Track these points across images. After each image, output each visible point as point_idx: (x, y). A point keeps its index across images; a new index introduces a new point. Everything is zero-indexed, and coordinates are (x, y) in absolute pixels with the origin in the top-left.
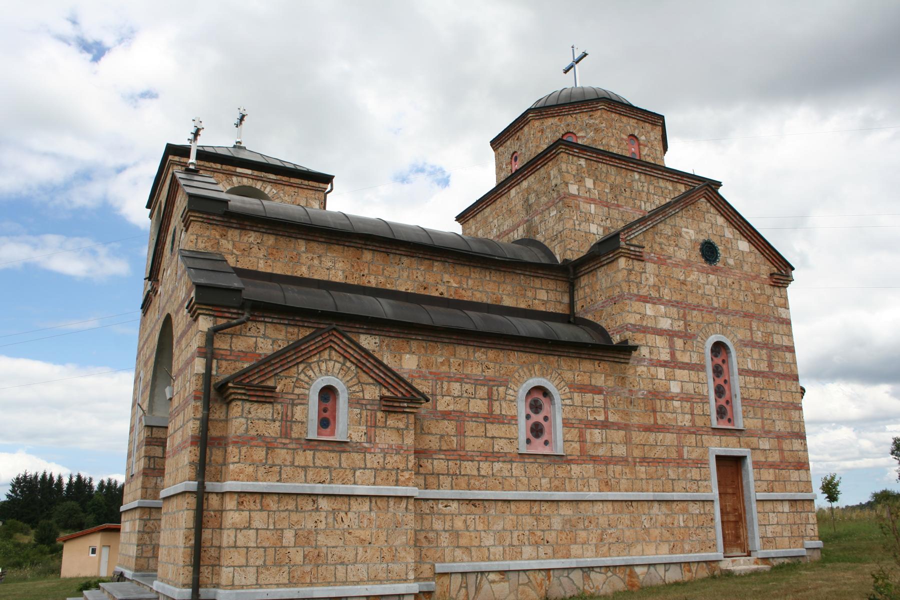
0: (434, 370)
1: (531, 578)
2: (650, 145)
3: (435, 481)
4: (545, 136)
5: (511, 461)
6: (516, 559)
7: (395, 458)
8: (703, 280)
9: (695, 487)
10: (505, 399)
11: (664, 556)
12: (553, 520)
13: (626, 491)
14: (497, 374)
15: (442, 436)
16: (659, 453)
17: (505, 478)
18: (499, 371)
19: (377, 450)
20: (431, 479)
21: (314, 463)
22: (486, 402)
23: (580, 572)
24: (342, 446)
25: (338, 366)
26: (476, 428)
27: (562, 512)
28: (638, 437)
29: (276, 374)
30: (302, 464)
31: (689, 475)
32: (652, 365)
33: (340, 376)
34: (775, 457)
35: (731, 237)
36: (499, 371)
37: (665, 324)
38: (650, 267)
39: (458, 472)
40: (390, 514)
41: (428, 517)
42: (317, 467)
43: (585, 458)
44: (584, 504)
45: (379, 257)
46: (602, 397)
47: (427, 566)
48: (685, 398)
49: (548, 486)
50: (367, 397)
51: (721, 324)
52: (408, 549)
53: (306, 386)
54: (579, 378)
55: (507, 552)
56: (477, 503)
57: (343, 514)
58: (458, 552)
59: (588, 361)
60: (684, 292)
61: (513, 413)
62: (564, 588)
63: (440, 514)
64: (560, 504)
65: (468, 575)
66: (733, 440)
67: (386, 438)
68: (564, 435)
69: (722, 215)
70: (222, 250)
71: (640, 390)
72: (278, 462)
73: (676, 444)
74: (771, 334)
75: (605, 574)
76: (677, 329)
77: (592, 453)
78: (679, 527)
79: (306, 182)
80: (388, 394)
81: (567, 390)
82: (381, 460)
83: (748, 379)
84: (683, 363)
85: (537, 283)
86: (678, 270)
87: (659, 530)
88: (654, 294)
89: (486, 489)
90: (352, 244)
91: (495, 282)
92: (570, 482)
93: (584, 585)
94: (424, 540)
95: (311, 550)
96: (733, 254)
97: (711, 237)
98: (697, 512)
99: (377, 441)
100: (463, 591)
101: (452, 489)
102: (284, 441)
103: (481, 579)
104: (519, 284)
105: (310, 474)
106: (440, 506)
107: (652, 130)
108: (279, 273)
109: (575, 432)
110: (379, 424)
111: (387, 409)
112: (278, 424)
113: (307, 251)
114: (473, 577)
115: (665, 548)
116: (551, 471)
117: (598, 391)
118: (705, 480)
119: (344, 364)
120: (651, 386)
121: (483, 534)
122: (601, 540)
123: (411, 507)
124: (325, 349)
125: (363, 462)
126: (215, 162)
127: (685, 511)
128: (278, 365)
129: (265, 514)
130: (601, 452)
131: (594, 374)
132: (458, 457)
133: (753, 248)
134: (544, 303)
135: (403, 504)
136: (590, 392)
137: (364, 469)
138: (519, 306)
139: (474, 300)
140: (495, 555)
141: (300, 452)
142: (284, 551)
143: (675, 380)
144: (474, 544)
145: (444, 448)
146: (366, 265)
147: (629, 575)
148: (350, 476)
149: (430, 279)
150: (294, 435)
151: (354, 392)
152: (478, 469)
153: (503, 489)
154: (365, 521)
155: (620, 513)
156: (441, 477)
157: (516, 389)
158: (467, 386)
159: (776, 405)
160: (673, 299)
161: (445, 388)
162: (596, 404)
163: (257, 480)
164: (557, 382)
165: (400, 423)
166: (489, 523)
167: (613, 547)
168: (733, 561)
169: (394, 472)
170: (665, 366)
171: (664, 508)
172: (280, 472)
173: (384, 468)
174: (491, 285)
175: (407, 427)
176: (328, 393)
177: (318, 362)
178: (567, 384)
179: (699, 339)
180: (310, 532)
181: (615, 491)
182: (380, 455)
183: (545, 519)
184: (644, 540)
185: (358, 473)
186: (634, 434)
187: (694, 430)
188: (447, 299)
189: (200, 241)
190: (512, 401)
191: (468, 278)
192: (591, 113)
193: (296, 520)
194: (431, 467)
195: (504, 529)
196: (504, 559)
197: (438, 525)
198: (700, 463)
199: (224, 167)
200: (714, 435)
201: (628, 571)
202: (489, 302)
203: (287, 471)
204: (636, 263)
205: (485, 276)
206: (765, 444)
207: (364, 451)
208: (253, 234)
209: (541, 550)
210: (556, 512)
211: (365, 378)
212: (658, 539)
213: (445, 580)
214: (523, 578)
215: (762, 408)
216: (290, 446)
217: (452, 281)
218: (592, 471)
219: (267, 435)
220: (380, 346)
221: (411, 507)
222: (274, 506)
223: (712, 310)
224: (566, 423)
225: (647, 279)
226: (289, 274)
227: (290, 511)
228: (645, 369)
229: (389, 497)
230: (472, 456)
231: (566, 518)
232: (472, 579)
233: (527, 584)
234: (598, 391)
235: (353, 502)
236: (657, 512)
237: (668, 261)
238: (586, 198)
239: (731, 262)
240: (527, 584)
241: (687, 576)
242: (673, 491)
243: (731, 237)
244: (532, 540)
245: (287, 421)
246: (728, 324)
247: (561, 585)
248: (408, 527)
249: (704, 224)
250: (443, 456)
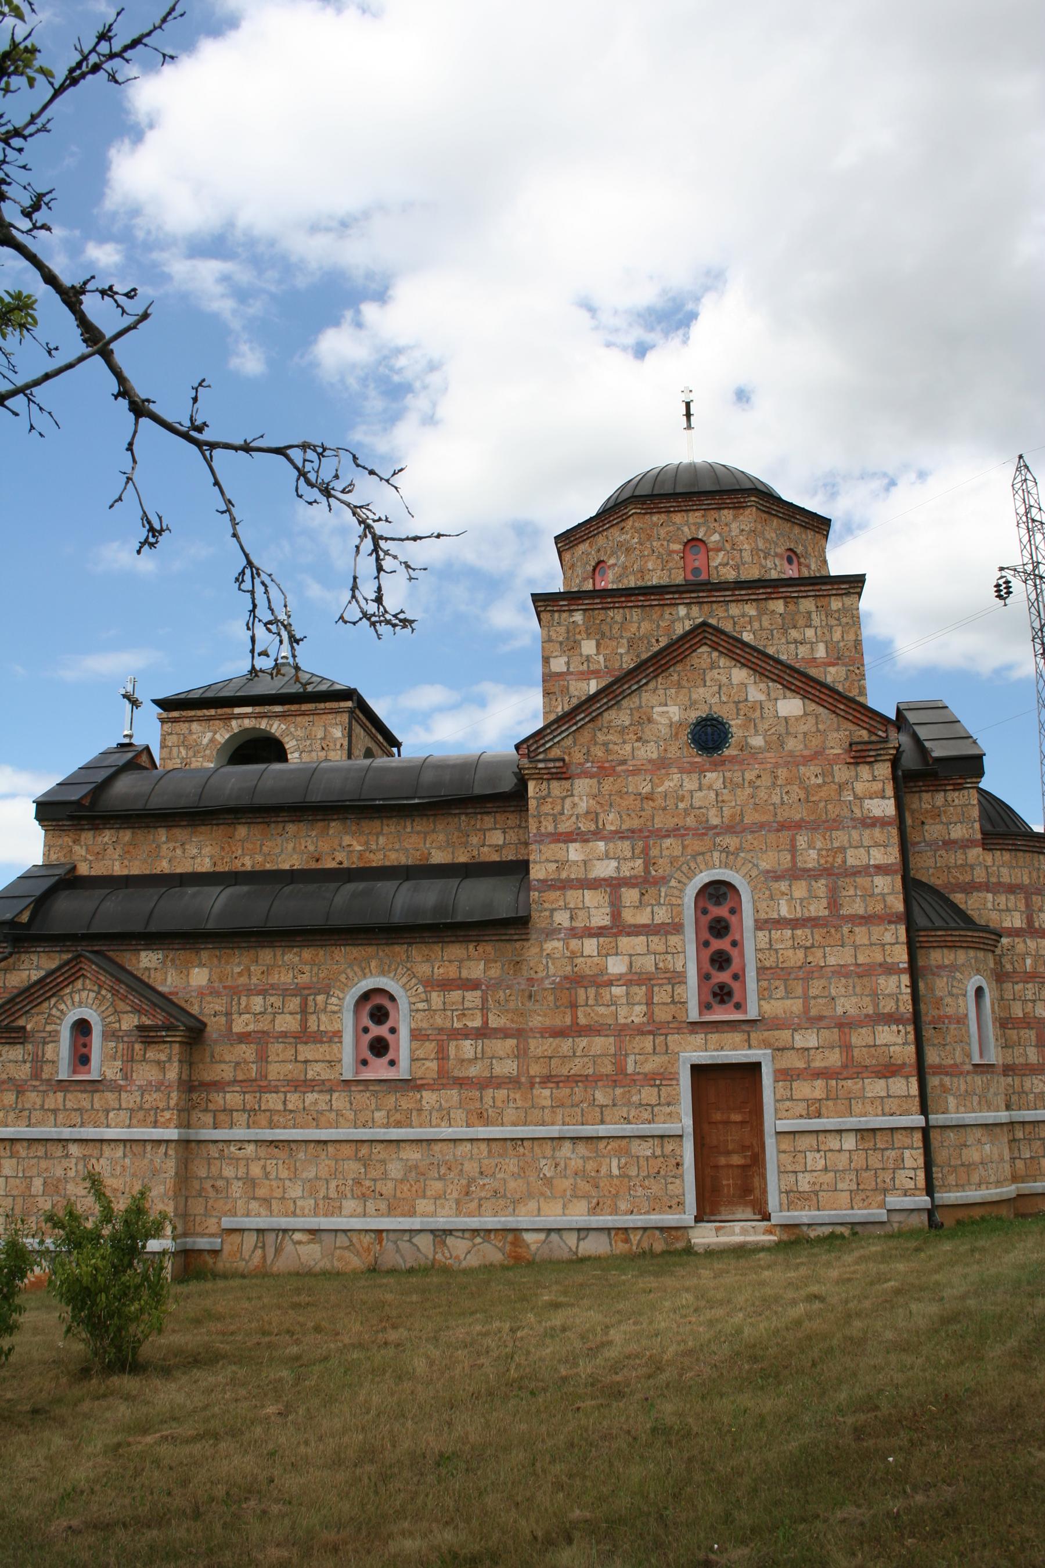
0: (229, 984)
1: (355, 1240)
2: (728, 546)
3: (227, 1119)
4: (575, 573)
5: (331, 1091)
6: (332, 1215)
7: (155, 1096)
8: (690, 783)
9: (646, 1115)
10: (325, 1010)
11: (578, 1216)
12: (390, 1166)
13: (514, 1124)
14: (315, 979)
15: (238, 1064)
16: (576, 1067)
17: (321, 1112)
18: (317, 974)
19: (134, 1088)
20: (222, 1117)
21: (64, 1106)
22: (299, 1017)
23: (431, 1237)
24: (94, 1086)
25: (92, 995)
26: (284, 1051)
27: (403, 1155)
28: (538, 1046)
29: (27, 1012)
30: (52, 1107)
31: (635, 1099)
32: (574, 936)
33: (94, 1007)
34: (834, 1059)
35: (762, 697)
36: (317, 974)
37: (605, 869)
38: (582, 786)
39: (257, 1107)
40: (146, 1161)
41: (216, 1161)
42: (67, 1110)
43: (444, 1081)
44: (440, 1145)
45: (256, 830)
46: (479, 993)
47: (214, 1220)
48: (634, 979)
49: (385, 1121)
50: (124, 1028)
51: (726, 850)
52: (166, 1201)
53: (58, 1021)
54: (441, 970)
55: (321, 1206)
56: (281, 1145)
57: (94, 1161)
58: (254, 1205)
59: (457, 946)
60: (648, 812)
61: (337, 1027)
62: (402, 1256)
63: (232, 1159)
64: (402, 1145)
65: (266, 1233)
66: (738, 1037)
67: (146, 1074)
68: (412, 1051)
69: (744, 665)
70: (76, 858)
71: (548, 976)
72: (27, 1106)
73: (612, 1051)
74: (842, 849)
75: (472, 1240)
76: (628, 874)
77: (457, 1073)
78: (611, 1176)
79: (322, 705)
80: (148, 1022)
81: (421, 989)
82: (138, 1099)
83: (776, 934)
84: (635, 926)
85: (488, 821)
86: (638, 778)
87: (572, 1181)
88: (585, 826)
89: (294, 1127)
90: (221, 821)
91: (418, 833)
92: (419, 1115)
93: (435, 1253)
94: (210, 1190)
95: (60, 1199)
96: (762, 726)
97: (715, 709)
98: (649, 1153)
99: (134, 1077)
100: (259, 1252)
101: (249, 1127)
102: (34, 1083)
103: (283, 1239)
104: (459, 829)
105: (61, 1116)
106: (232, 1149)
107: (735, 517)
108: (136, 873)
109: (430, 1047)
110: (137, 1058)
111: (144, 1039)
112: (28, 1065)
113: (168, 840)
114: (273, 1235)
115: (582, 1206)
116: (391, 1100)
117: (473, 985)
118: (669, 1104)
119: (98, 993)
120: (569, 968)
121: (287, 1182)
122: (467, 1194)
123: (171, 1152)
124: (78, 978)
125: (117, 1102)
126: (208, 708)
127: (619, 1153)
128: (25, 1003)
129: (14, 1161)
130: (473, 1071)
131: (467, 963)
132: (257, 1089)
133: (813, 706)
134: (498, 849)
135: (162, 1149)
136: (458, 988)
137: (118, 1110)
138: (456, 861)
139: (387, 863)
140: (303, 1209)
141: (51, 1094)
142: (32, 1200)
143: (617, 954)
144: (275, 1195)
145: (240, 1078)
146: (240, 843)
147: (512, 1243)
148: (103, 1119)
149: (324, 846)
150: (45, 1076)
151: (110, 1023)
152: (285, 1103)
153: (317, 1127)
154: (119, 1169)
155: (500, 1155)
156: (235, 1114)
157: (341, 995)
158: (272, 999)
159: (841, 972)
160: (624, 827)
161: (243, 1003)
162: (467, 1004)
163: (7, 1126)
164: (404, 980)
165: (161, 1054)
166: (296, 1170)
167: (486, 1204)
168: (718, 1229)
169: (152, 1113)
170: (597, 935)
171: (582, 1149)
172: (29, 1117)
173: (141, 1108)
174: (414, 839)
175: (170, 1059)
176: (82, 1027)
177: (71, 993)
178: (420, 982)
179: (673, 883)
180: (59, 1180)
181: (493, 1125)
182: (137, 1094)
183: (378, 1165)
184: (542, 1194)
185: (111, 1115)
186: (533, 1043)
187: (653, 1028)
188: (349, 869)
189: (52, 852)
190: (334, 1012)
191: (381, 833)
192: (622, 524)
193: (44, 1167)
194: (222, 1102)
195: (317, 1178)
196: (316, 1215)
197: (228, 1172)
198: (661, 1079)
199: (220, 711)
200: (692, 1032)
201: (510, 1237)
202: (410, 862)
203: (37, 1115)
204: (555, 784)
205: (405, 827)
206: (808, 1039)
207: (120, 1089)
208: (107, 833)
209: (371, 1206)
210: (394, 1156)
211: (122, 1006)
212: (568, 1193)
213: (236, 1238)
214: (342, 1240)
215: (807, 979)
216: (41, 1088)
217: (355, 843)
218: (456, 1098)
219: (17, 1077)
220: (164, 963)
221: (171, 1152)
222: (23, 1153)
223: (705, 830)
224: (416, 1035)
225: (575, 805)
226: (147, 872)
227: (39, 1157)
228: (559, 944)
229: (145, 1141)
230: (276, 1086)
231: (410, 1163)
232: (270, 1238)
233: (347, 1248)
234: (473, 985)
235: (105, 1147)
236: (568, 1155)
237: (619, 768)
238: (582, 673)
239: (757, 741)
240: (347, 1248)
241: (621, 1247)
242: (602, 1122)
243: (762, 697)
244: (358, 1192)
245: (37, 1061)
246: (740, 849)
247: (398, 1251)
248: (167, 1175)
249: (701, 690)
250: (238, 1089)
